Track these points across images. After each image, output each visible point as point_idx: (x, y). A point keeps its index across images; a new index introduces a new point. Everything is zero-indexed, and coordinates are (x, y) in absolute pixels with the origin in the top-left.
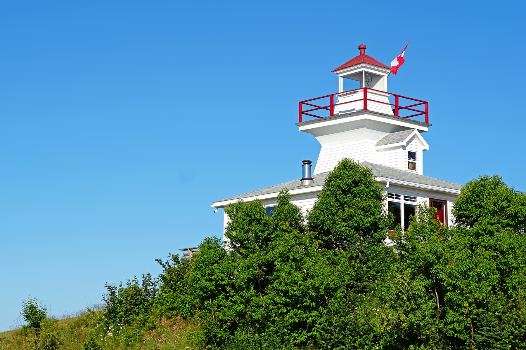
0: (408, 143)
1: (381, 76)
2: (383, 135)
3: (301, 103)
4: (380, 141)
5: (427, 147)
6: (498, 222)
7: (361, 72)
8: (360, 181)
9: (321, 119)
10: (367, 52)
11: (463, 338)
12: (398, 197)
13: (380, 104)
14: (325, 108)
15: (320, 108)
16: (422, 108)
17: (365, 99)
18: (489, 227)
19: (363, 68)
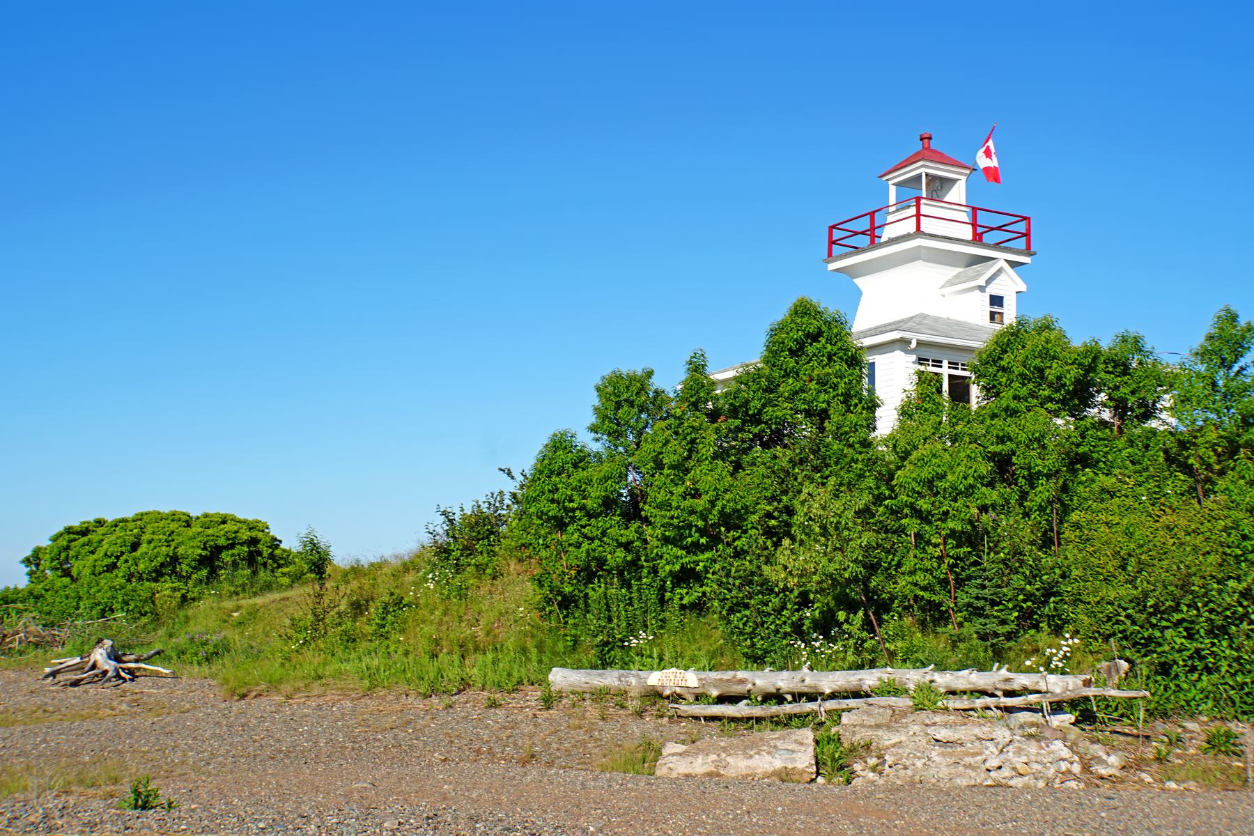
0: (989, 281)
1: (955, 181)
2: (952, 272)
3: (832, 227)
4: (948, 281)
5: (1023, 287)
6: (1033, 395)
7: (920, 176)
8: (820, 333)
9: (857, 250)
10: (934, 145)
11: (936, 598)
12: (937, 363)
13: (948, 220)
14: (863, 233)
15: (856, 233)
16: (1021, 227)
17: (918, 215)
18: (1013, 404)
19: (922, 169)
